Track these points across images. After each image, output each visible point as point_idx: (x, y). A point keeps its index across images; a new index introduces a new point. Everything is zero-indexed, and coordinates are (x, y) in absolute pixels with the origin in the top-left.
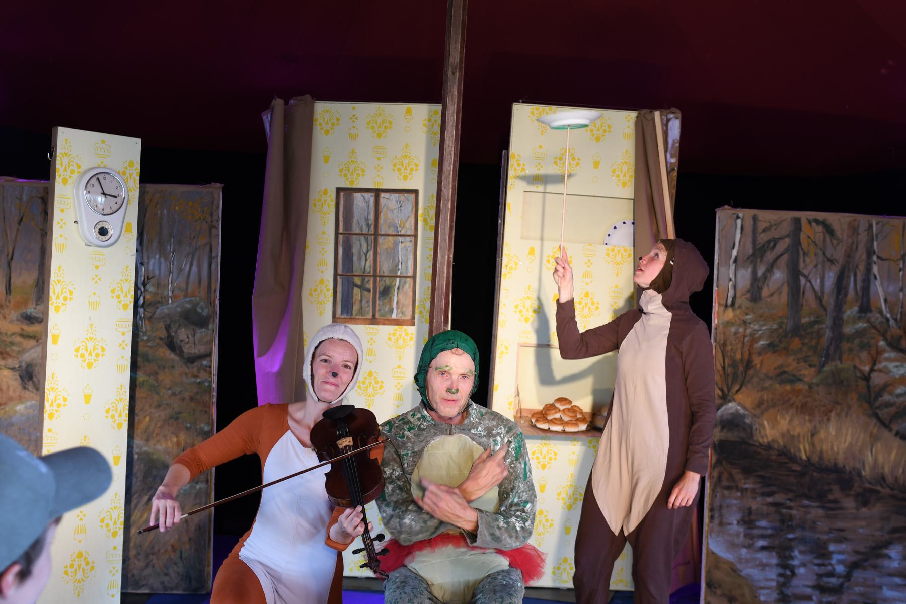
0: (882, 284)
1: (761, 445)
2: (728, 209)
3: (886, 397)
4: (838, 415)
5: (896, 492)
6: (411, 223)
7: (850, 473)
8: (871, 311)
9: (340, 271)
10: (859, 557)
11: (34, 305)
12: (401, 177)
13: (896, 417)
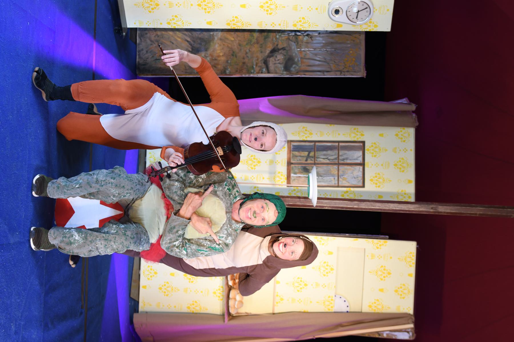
9: (317, 144)
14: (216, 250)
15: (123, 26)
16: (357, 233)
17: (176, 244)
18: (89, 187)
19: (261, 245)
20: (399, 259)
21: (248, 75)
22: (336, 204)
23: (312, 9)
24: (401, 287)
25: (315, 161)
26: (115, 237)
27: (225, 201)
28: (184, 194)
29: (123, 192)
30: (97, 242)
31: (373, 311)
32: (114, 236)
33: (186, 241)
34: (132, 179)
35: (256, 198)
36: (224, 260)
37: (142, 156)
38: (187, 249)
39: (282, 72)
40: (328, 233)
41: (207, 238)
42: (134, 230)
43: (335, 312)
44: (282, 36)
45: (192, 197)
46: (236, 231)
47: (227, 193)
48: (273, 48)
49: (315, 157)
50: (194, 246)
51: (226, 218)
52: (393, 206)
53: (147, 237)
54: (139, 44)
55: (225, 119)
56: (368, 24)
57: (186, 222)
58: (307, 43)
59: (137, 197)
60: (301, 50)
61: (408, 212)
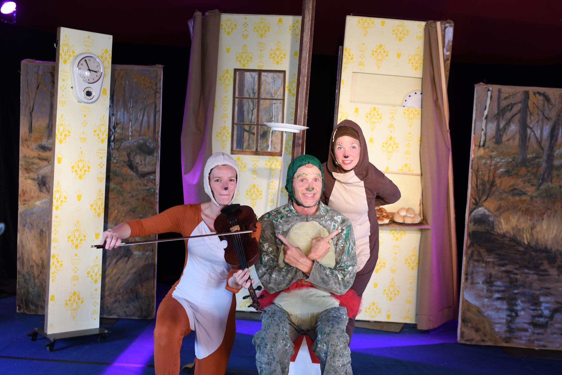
1: (499, 234)
2: (483, 85)
4: (549, 217)
6: (281, 91)
7: (555, 253)
9: (236, 122)
10: (559, 305)
11: (46, 139)
14: (348, 234)
15: (97, 332)
16: (336, 80)
17: (341, 277)
18: (275, 373)
19: (344, 182)
20: (365, 36)
21: (157, 195)
22: (303, 101)
23: (85, 122)
24: (396, 34)
25: (255, 125)
26: (331, 345)
27: (295, 223)
28: (285, 268)
29: (282, 335)
30: (336, 365)
31: (422, 65)
32: (330, 346)
33: (338, 266)
34: (267, 325)
35: (292, 187)
36: (360, 225)
37: (243, 315)
38: (347, 266)
39: (155, 158)
40: (335, 112)
41: (335, 243)
42: (324, 323)
43: (422, 108)
44: (114, 156)
45: (289, 257)
46: (328, 211)
47: (286, 219)
48: (127, 167)
49: (250, 125)
50: (343, 258)
51: (313, 221)
52: (306, 38)
53: (332, 310)
54: (119, 316)
55: (203, 221)
56: (104, 60)
57: (317, 266)
58: (123, 128)
59: (287, 319)
60: (131, 136)
61: (314, 22)
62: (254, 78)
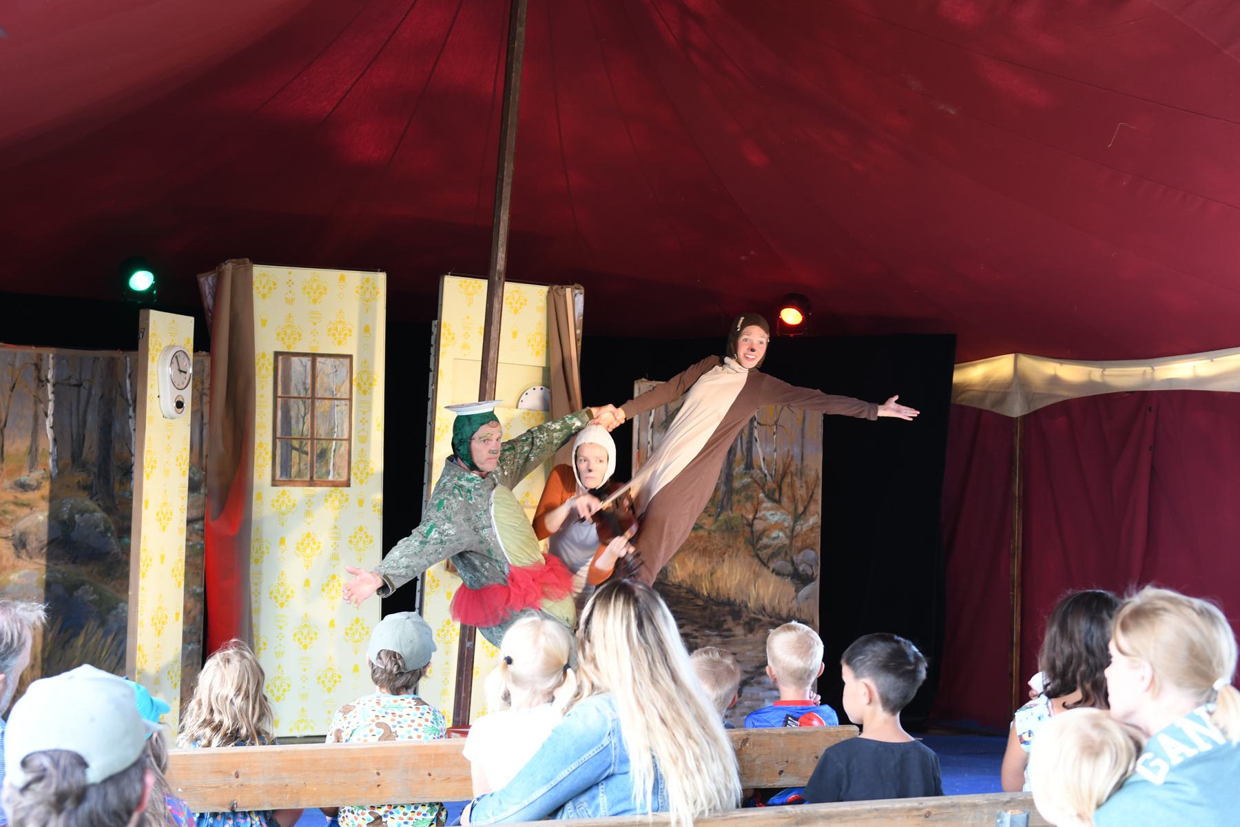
0: (761, 446)
1: (674, 585)
2: (646, 382)
3: (765, 541)
4: (730, 556)
5: (773, 619)
7: (740, 605)
8: (753, 468)
9: (279, 434)
10: (748, 676)
11: (28, 471)
12: (336, 342)
13: (773, 556)
62: (306, 366)
